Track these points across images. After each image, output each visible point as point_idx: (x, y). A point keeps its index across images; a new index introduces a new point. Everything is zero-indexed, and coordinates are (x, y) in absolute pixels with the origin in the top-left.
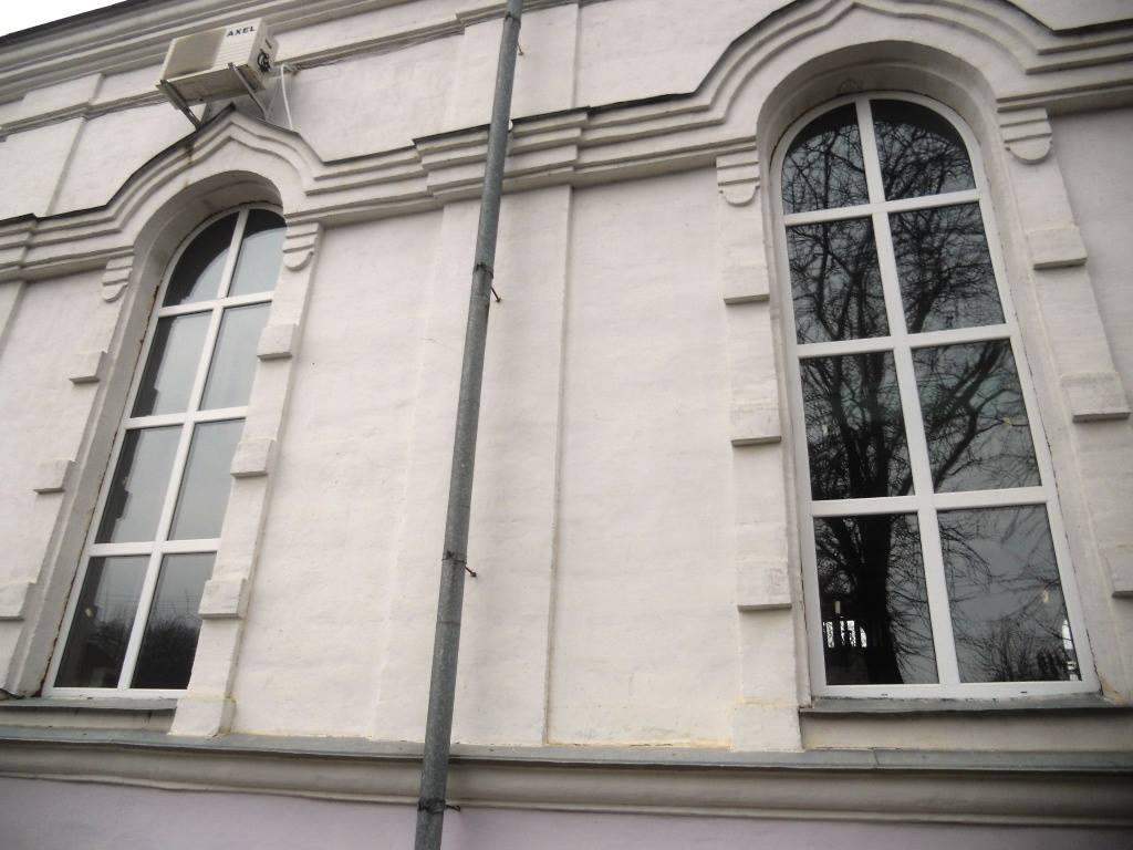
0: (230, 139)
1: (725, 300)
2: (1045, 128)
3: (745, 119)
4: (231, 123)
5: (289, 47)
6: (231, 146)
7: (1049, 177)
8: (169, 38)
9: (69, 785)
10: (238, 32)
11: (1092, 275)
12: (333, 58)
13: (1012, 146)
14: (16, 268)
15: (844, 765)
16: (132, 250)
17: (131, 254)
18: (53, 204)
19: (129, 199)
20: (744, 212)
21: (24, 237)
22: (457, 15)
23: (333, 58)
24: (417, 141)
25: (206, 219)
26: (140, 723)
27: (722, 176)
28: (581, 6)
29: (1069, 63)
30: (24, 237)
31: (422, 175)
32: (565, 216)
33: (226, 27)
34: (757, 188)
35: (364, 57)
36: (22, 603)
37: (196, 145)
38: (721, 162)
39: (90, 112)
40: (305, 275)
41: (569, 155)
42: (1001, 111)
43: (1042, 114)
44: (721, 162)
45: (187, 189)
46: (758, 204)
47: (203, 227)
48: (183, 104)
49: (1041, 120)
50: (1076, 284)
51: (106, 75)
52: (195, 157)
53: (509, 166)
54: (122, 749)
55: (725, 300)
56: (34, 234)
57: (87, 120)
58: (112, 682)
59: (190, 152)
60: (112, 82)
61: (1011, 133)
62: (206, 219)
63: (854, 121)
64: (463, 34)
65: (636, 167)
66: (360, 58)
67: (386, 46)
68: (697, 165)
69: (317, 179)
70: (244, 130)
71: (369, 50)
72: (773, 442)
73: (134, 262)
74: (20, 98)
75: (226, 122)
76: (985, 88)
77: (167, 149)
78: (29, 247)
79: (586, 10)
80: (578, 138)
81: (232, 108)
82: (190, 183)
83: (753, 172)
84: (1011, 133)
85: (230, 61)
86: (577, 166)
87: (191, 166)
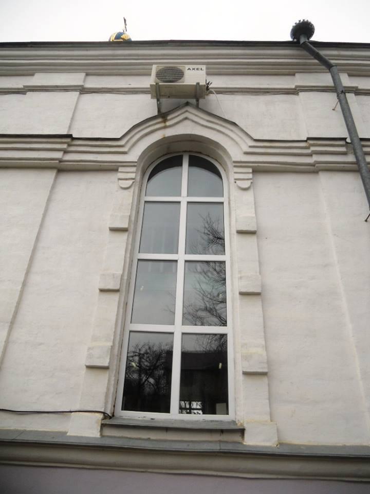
0: (186, 118)
1: (109, 228)
2: (250, 176)
3: (134, 155)
4: (187, 111)
5: (217, 82)
6: (187, 122)
7: (249, 196)
8: (152, 64)
9: (173, 477)
10: (194, 69)
11: (258, 238)
12: (230, 92)
13: (237, 181)
14: (57, 161)
15: (212, 450)
16: (136, 164)
17: (135, 166)
18: (68, 132)
19: (131, 138)
20: (126, 192)
22: (24, 86)
23: (230, 92)
24: (309, 139)
25: (164, 155)
26: (217, 437)
27: (120, 175)
28: (81, 94)
29: (298, 153)
30: (65, 146)
31: (310, 155)
32: (52, 181)
33: (187, 66)
34: (133, 182)
35: (245, 95)
36: (109, 357)
37: (169, 118)
38: (120, 169)
39: (83, 90)
40: (251, 193)
41: (58, 155)
42: (235, 166)
43: (250, 170)
44: (120, 169)
45: (165, 139)
46: (132, 190)
47: (162, 159)
48: (158, 97)
49: (250, 173)
50: (252, 240)
51: (87, 75)
52: (168, 124)
54: (222, 454)
55: (109, 228)
56: (69, 145)
57: (81, 94)
58: (167, 410)
59: (165, 121)
60: (90, 78)
61: (238, 176)
62: (164, 155)
63: (180, 164)
64: (25, 94)
65: (264, 166)
66: (243, 95)
67: (268, 92)
69: (250, 147)
70: (191, 113)
71: (248, 92)
72: (117, 291)
73: (137, 170)
74: (33, 75)
75: (183, 110)
76: (230, 157)
77: (146, 120)
78: (66, 152)
79: (82, 95)
80: (65, 148)
81: (187, 104)
82: (166, 136)
83: (133, 175)
84: (238, 176)
85: (198, 81)
86: (61, 161)
87: (165, 127)
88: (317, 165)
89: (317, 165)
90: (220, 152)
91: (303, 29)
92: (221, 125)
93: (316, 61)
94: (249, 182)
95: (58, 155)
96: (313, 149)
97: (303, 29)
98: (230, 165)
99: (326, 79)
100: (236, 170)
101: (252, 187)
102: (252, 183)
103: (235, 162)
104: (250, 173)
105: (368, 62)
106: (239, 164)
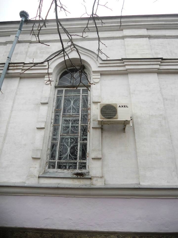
2: (99, 77)
21: (159, 63)
30: (159, 63)
41: (158, 67)
42: (93, 73)
43: (99, 74)
49: (99, 75)
53: (10, 71)
56: (23, 67)
68: (41, 76)
74: (9, 36)
86: (159, 69)
89: (128, 70)
90: (89, 67)
91: (23, 14)
92: (90, 54)
93: (64, 27)
94: (99, 79)
95: (158, 67)
96: (125, 63)
97: (23, 14)
98: (92, 73)
99: (95, 35)
100: (93, 74)
101: (100, 82)
102: (100, 80)
103: (93, 71)
104: (99, 75)
105: (177, 23)
106: (94, 72)
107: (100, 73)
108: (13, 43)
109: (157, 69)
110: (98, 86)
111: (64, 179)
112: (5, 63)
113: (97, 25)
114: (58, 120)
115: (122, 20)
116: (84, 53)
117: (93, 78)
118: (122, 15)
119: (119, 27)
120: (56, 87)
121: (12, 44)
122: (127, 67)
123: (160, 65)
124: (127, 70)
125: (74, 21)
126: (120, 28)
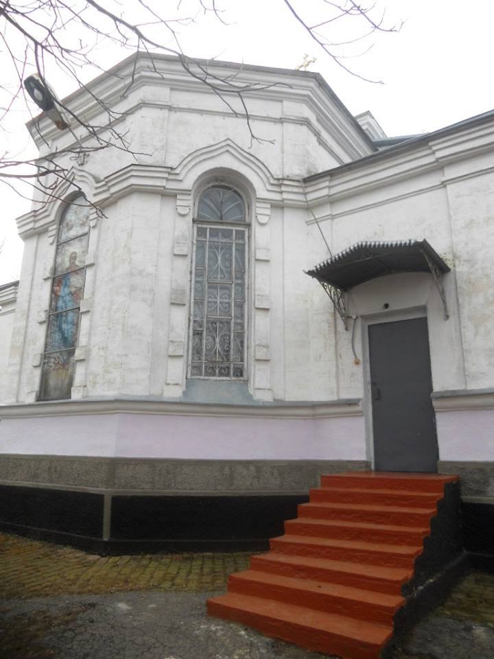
2: (268, 212)
43: (269, 206)
88: (286, 202)
90: (249, 190)
94: (267, 218)
107: (271, 203)
108: (19, 228)
109: (162, 189)
110: (266, 230)
111: (217, 389)
112: (19, 279)
113: (76, 114)
114: (210, 295)
115: (85, 115)
116: (239, 156)
117: (261, 212)
118: (34, 117)
119: (87, 117)
120: (194, 221)
121: (12, 315)
122: (285, 196)
123: (167, 179)
124: (283, 200)
125: (274, 75)
126: (85, 117)
